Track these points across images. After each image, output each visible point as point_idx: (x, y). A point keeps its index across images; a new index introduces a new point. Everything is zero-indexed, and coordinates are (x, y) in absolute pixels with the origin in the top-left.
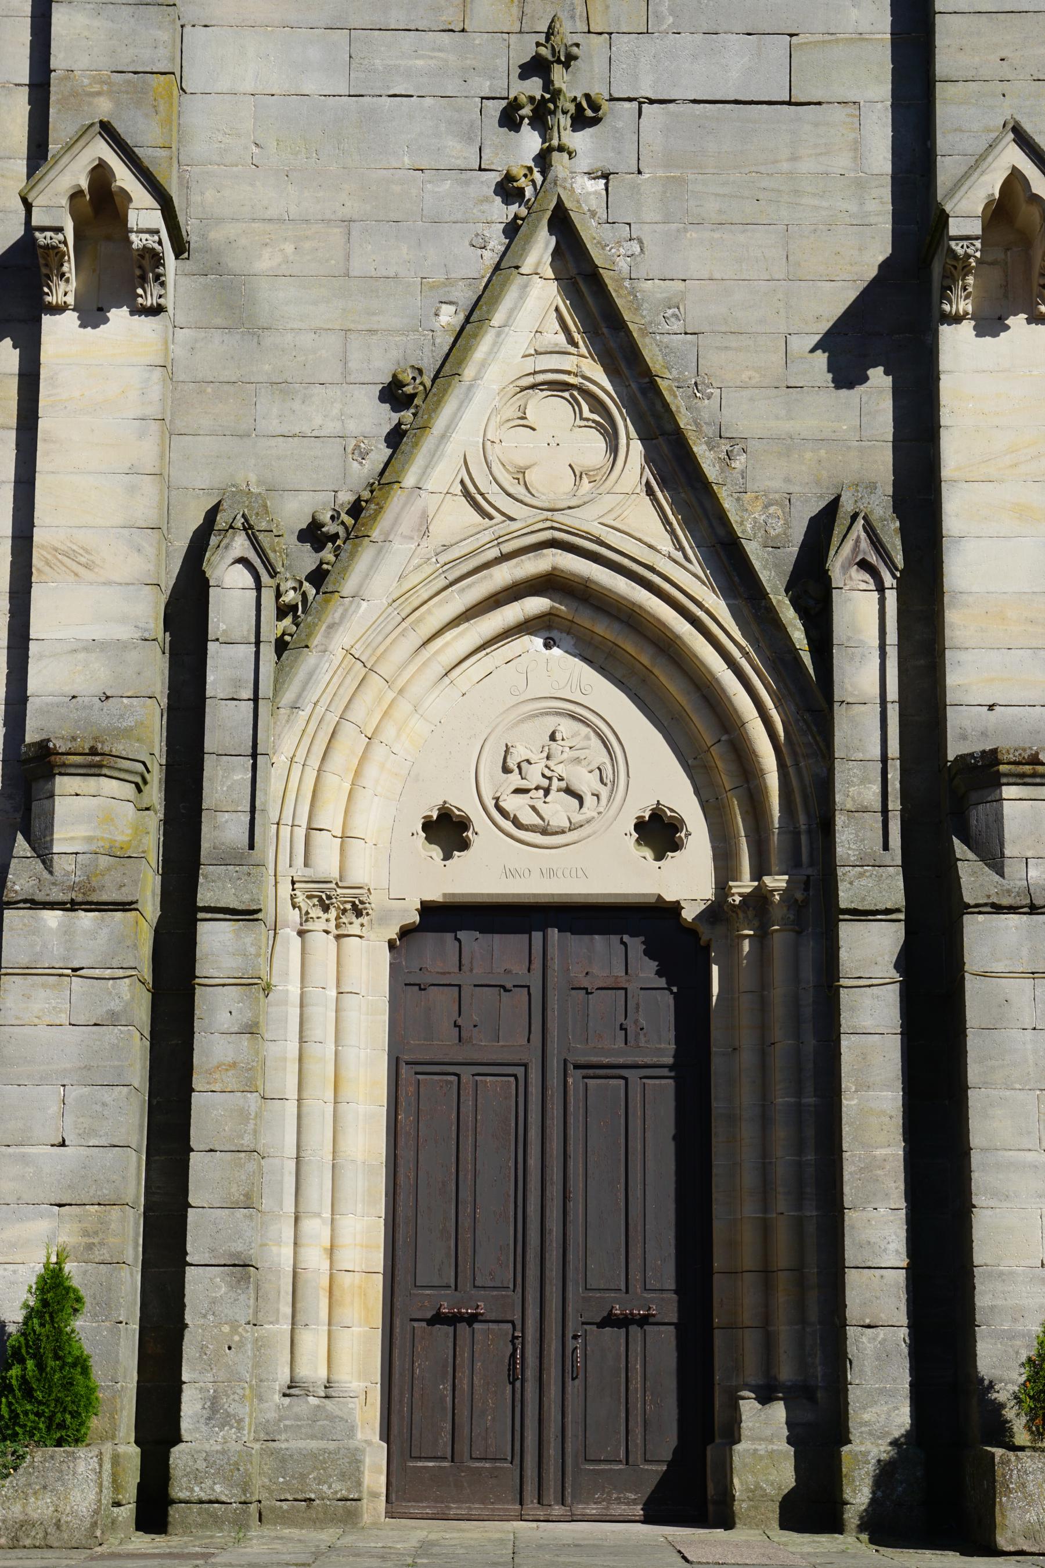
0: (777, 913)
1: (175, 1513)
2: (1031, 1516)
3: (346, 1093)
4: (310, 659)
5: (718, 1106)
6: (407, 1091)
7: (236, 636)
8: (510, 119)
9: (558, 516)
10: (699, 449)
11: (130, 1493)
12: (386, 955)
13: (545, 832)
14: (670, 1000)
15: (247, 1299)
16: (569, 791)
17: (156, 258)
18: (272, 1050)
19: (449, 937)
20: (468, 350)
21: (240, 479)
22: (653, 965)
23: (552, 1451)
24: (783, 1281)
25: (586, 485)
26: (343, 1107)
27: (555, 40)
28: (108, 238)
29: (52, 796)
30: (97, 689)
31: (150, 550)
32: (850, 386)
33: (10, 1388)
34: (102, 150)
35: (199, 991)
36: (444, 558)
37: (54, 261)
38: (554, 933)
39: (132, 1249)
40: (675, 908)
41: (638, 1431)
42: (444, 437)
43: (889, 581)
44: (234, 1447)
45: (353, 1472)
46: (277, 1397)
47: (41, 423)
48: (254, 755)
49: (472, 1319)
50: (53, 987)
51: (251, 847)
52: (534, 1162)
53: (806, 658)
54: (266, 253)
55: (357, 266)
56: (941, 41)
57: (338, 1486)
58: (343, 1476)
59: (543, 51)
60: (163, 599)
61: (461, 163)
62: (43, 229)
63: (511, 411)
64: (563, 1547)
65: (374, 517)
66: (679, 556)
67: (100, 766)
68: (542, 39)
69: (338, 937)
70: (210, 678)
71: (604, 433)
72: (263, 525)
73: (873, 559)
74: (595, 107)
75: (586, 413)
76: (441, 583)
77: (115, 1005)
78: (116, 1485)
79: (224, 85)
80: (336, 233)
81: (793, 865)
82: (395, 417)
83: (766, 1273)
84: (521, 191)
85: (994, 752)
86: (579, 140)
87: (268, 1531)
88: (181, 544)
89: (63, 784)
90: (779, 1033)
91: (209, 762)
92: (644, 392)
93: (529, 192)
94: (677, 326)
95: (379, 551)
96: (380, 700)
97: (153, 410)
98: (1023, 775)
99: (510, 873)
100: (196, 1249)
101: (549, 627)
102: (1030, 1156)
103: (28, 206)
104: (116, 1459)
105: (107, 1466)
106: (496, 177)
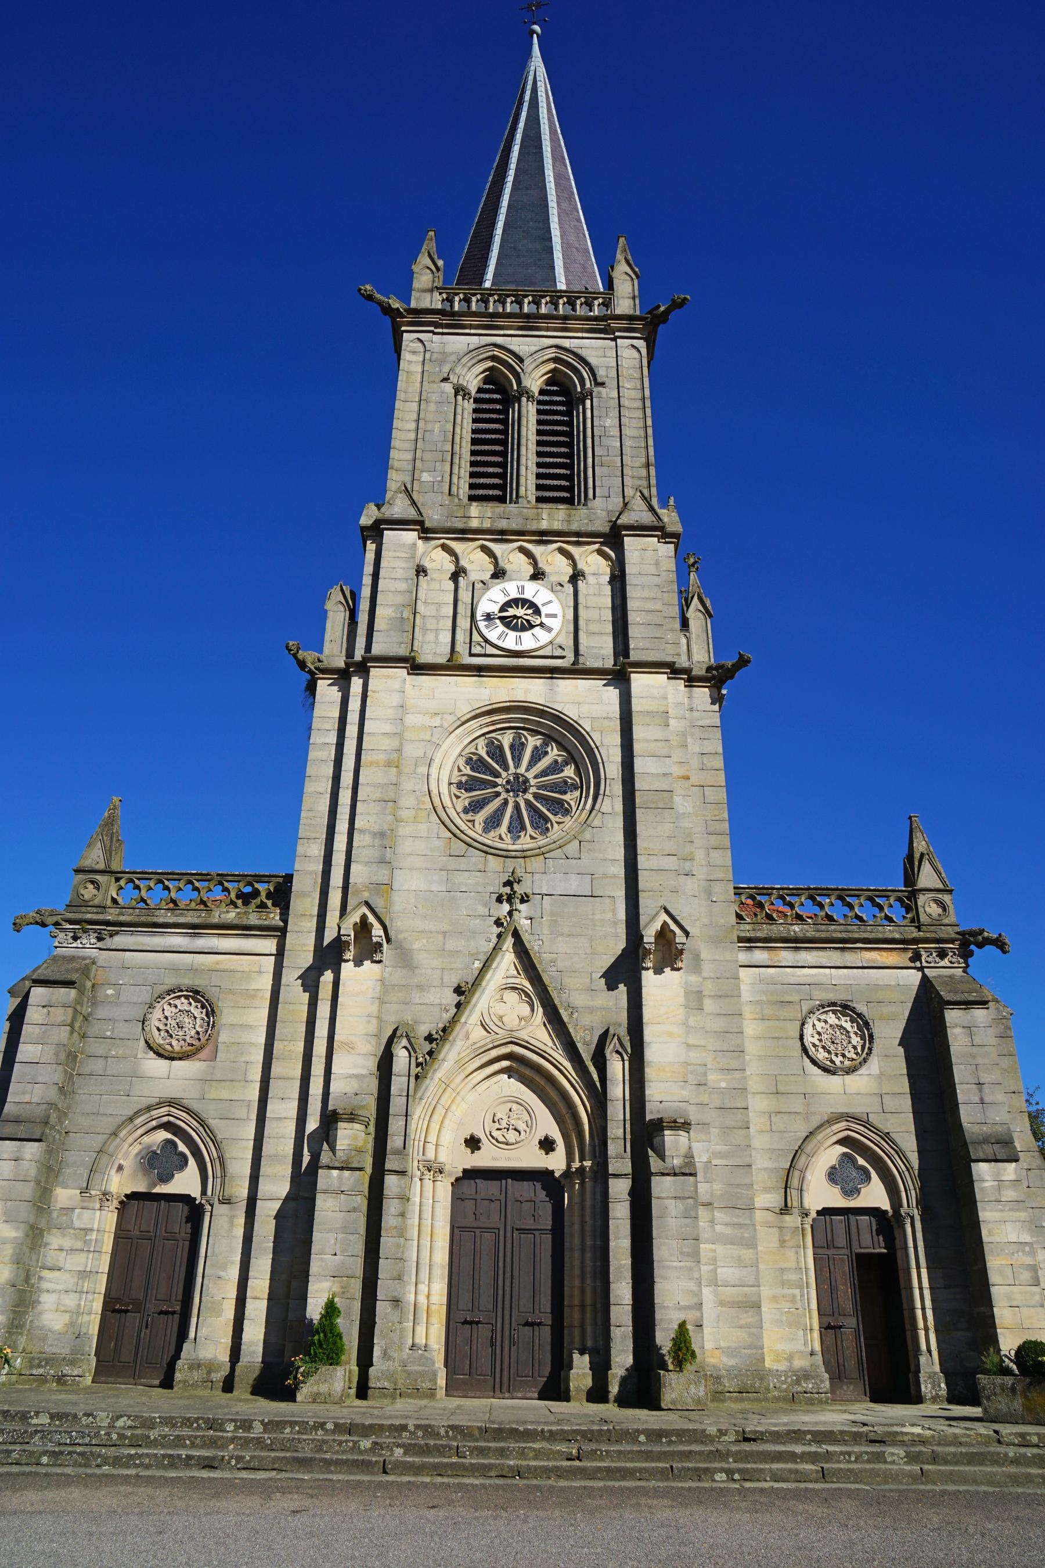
0: (588, 1175)
1: (370, 1392)
2: (673, 1396)
3: (435, 1238)
4: (427, 1081)
5: (567, 1244)
6: (456, 1238)
7: (401, 1074)
8: (499, 900)
9: (513, 1033)
10: (562, 1011)
11: (354, 1385)
12: (450, 1188)
13: (507, 1144)
14: (550, 1205)
15: (398, 1313)
16: (515, 1129)
17: (380, 945)
18: (409, 1222)
19: (472, 1181)
20: (483, 977)
21: (405, 1018)
22: (545, 1193)
23: (506, 1373)
24: (589, 1309)
25: (523, 1022)
26: (433, 1243)
27: (515, 875)
28: (365, 937)
29: (337, 1129)
30: (353, 1091)
31: (374, 1043)
32: (613, 990)
33: (314, 1343)
34: (365, 910)
35: (384, 1200)
36: (474, 1047)
37: (347, 945)
38: (509, 1181)
39: (358, 1294)
40: (553, 1172)
41: (536, 1365)
42: (475, 1005)
43: (626, 1058)
44: (392, 1368)
45: (434, 1379)
46: (407, 1350)
47: (339, 999)
48: (406, 1116)
49: (126, 1311)
50: (334, 1198)
51: (404, 1148)
52: (501, 1265)
53: (598, 1084)
54: (417, 942)
55: (448, 947)
56: (640, 878)
57: (428, 1384)
58: (430, 1380)
59: (511, 879)
60: (378, 1060)
61: (483, 914)
62: (344, 935)
63: (498, 997)
64: (508, 1407)
65: (450, 1033)
66: (554, 1047)
67: (353, 1119)
68: (510, 874)
69: (434, 1181)
70: (392, 1088)
71: (530, 1005)
72: (412, 1035)
73: (620, 1050)
74: (528, 897)
75: (524, 998)
76: (473, 1056)
77: (355, 1205)
78: (350, 1381)
79: (405, 887)
80: (440, 937)
81: (593, 1158)
82: (459, 998)
83: (583, 1307)
84: (503, 923)
85: (662, 1118)
86: (522, 907)
87: (403, 1400)
88: (384, 1041)
89: (341, 1125)
90: (588, 1218)
91: (391, 1118)
92: (543, 991)
93: (505, 924)
94: (554, 969)
95: (452, 1044)
96: (450, 1096)
97: (377, 995)
98: (671, 1127)
99: (494, 1159)
100: (380, 1295)
101: (510, 1071)
102: (675, 1264)
103: (339, 928)
104: (350, 1371)
105: (347, 1374)
106: (494, 919)
